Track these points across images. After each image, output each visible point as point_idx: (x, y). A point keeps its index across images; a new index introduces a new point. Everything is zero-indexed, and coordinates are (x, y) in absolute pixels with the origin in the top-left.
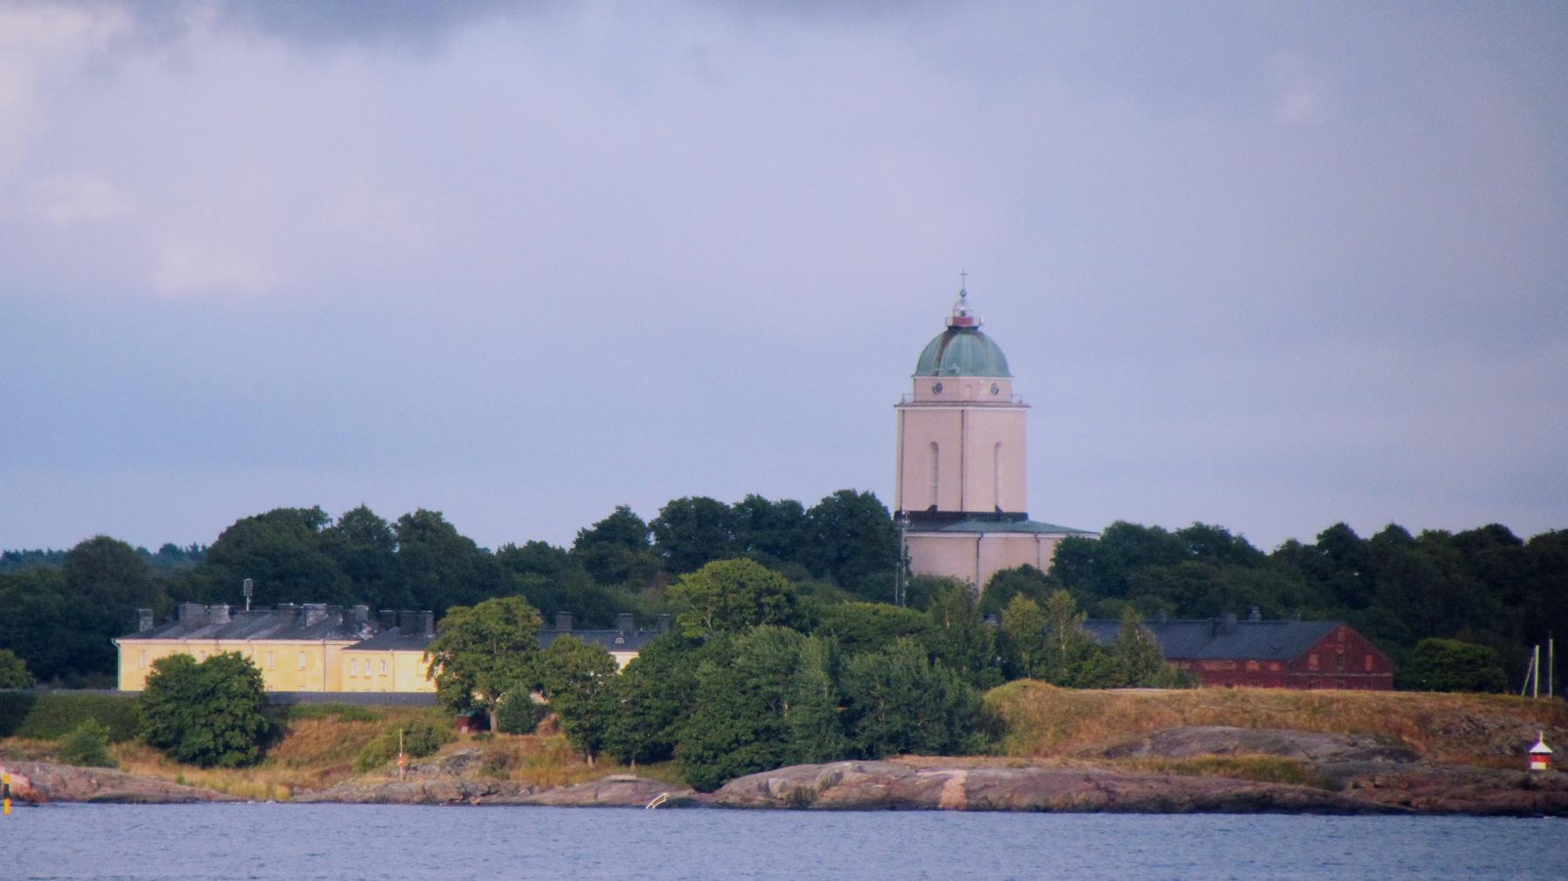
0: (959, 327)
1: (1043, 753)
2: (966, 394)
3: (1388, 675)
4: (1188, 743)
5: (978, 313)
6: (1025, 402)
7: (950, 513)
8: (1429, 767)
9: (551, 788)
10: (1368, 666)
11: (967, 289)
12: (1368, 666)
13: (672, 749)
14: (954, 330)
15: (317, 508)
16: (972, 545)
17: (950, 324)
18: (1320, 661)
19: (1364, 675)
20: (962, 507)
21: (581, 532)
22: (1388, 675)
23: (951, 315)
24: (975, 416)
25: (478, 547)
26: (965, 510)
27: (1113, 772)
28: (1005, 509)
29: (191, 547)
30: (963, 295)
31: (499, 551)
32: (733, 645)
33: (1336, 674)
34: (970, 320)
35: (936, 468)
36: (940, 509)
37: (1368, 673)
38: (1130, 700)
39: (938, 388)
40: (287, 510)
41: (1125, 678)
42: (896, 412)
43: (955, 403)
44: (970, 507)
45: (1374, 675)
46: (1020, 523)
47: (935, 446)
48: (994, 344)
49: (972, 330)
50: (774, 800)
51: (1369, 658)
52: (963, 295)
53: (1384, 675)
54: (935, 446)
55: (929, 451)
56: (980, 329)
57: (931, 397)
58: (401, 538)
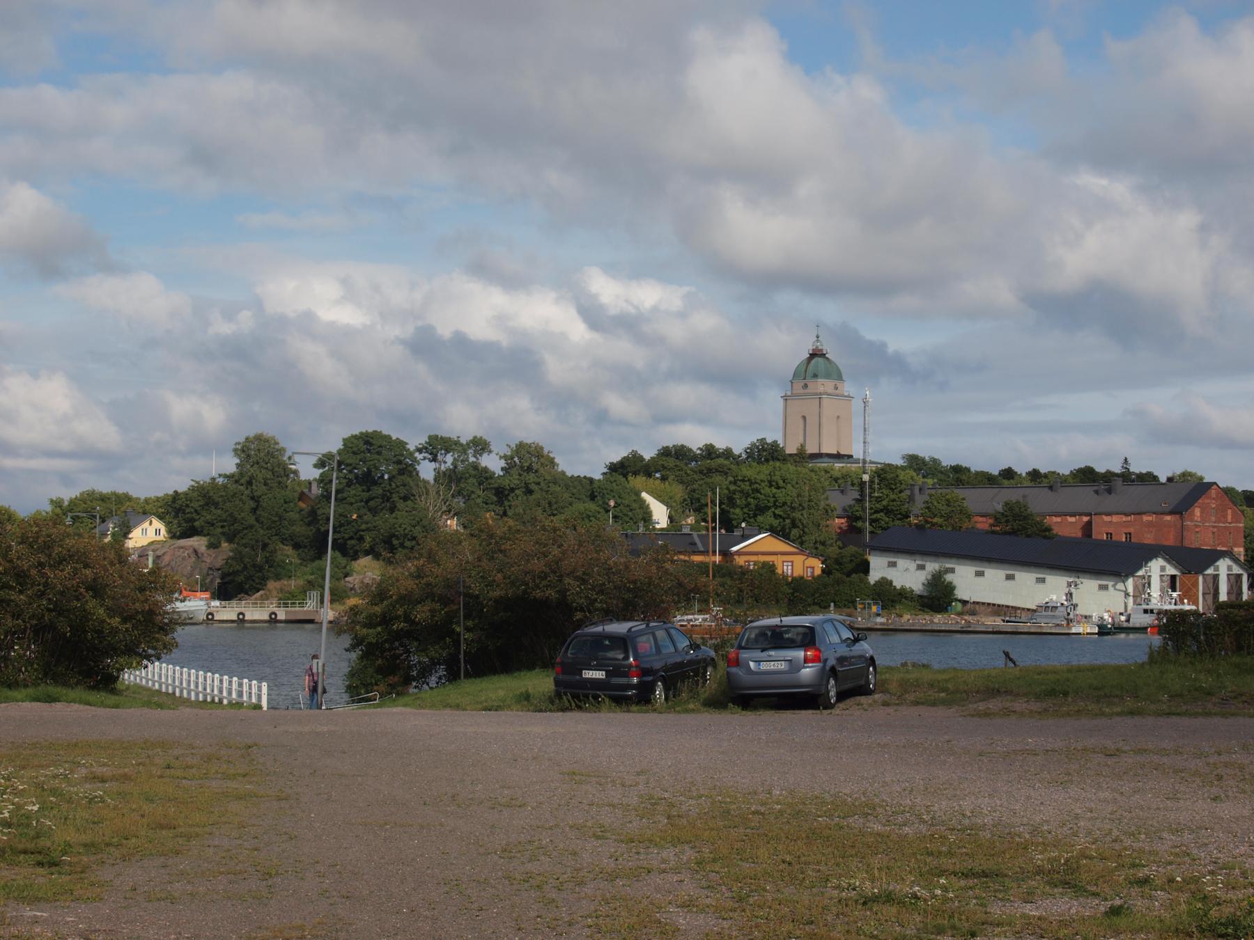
0: (815, 354)
1: (829, 475)
2: (821, 389)
3: (1241, 525)
6: (851, 395)
7: (815, 454)
8: (270, 473)
9: (93, 716)
10: (1229, 517)
12: (1229, 517)
13: (351, 645)
14: (813, 355)
15: (344, 440)
16: (818, 401)
17: (811, 352)
18: (1201, 512)
19: (1228, 525)
22: (1241, 525)
23: (811, 348)
24: (826, 401)
28: (842, 452)
33: (1211, 524)
35: (805, 430)
37: (1230, 523)
39: (806, 386)
42: (782, 400)
43: (816, 394)
44: (824, 451)
45: (1232, 525)
46: (851, 459)
47: (804, 418)
48: (837, 366)
49: (823, 355)
50: (1013, 495)
51: (1229, 512)
53: (1238, 525)
54: (804, 418)
55: (801, 421)
56: (827, 356)
57: (802, 391)
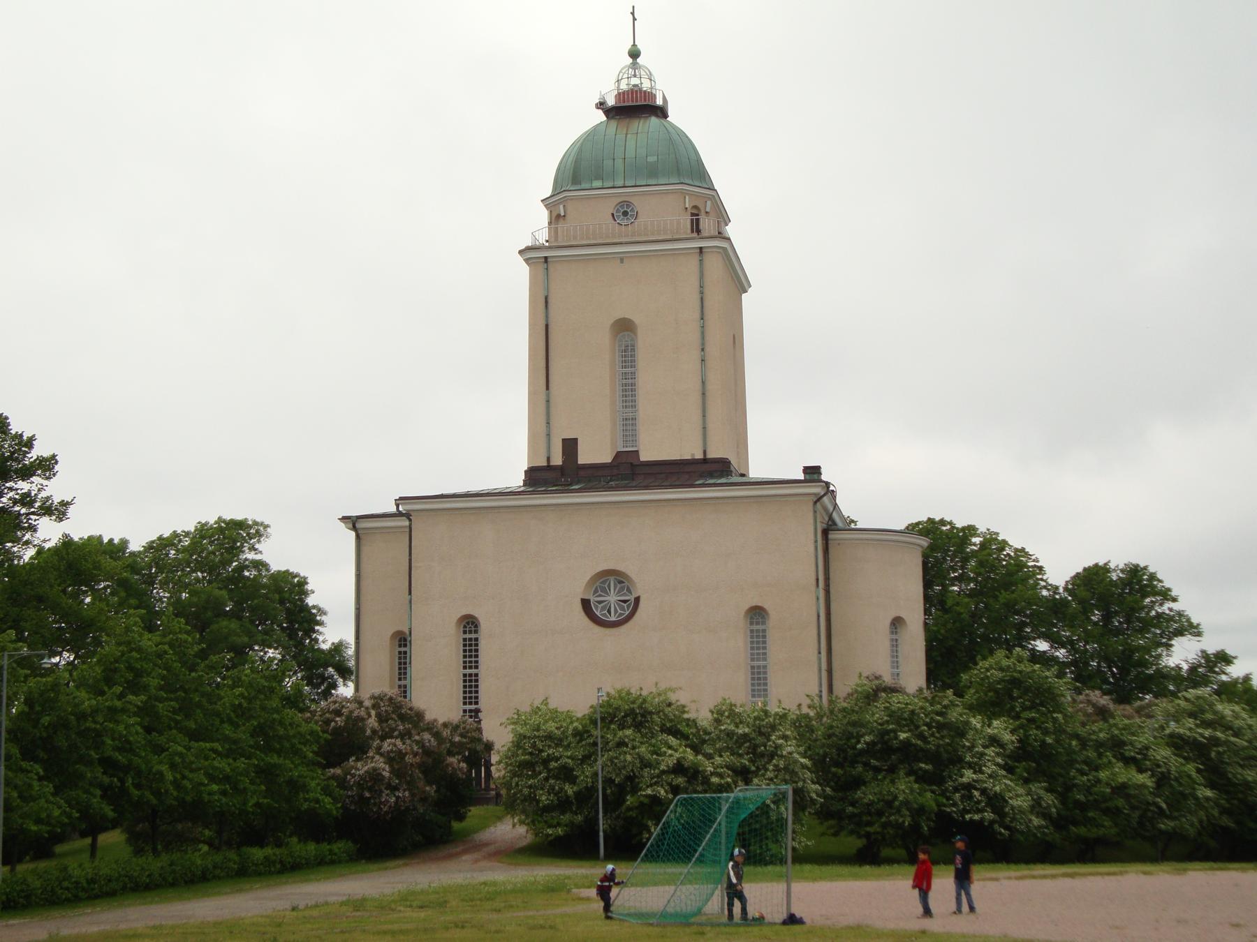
4: (727, 767)
5: (665, 88)
11: (640, 46)
20: (548, 459)
21: (324, 618)
25: (135, 546)
26: (711, 455)
27: (1200, 692)
29: (9, 422)
30: (634, 54)
31: (111, 540)
32: (1058, 708)
34: (650, 95)
36: (645, 457)
38: (793, 723)
39: (625, 211)
40: (926, 645)
41: (110, 825)
52: (634, 54)
58: (750, 776)
